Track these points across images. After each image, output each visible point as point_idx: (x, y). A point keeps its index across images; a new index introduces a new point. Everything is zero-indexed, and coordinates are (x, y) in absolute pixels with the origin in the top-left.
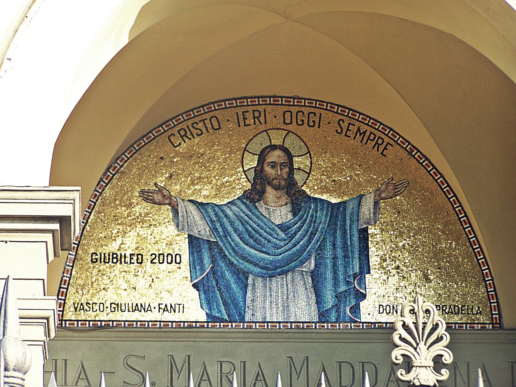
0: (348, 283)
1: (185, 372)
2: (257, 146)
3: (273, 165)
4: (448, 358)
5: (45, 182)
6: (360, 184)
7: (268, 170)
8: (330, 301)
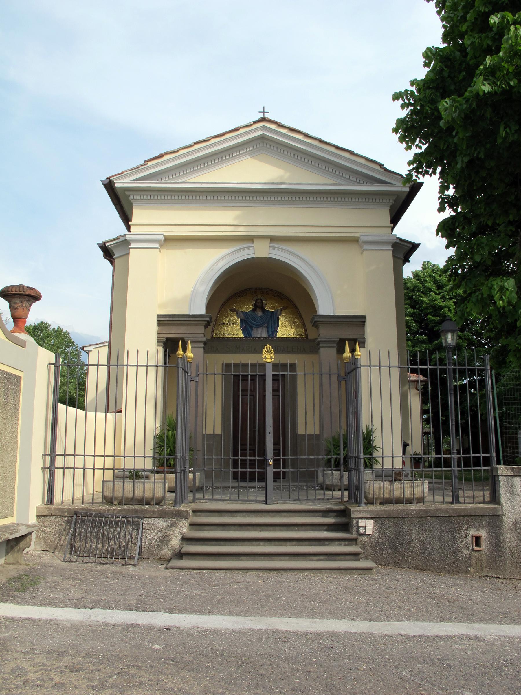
0: (275, 329)
2: (256, 298)
3: (258, 303)
4: (273, 357)
6: (277, 307)
8: (270, 333)
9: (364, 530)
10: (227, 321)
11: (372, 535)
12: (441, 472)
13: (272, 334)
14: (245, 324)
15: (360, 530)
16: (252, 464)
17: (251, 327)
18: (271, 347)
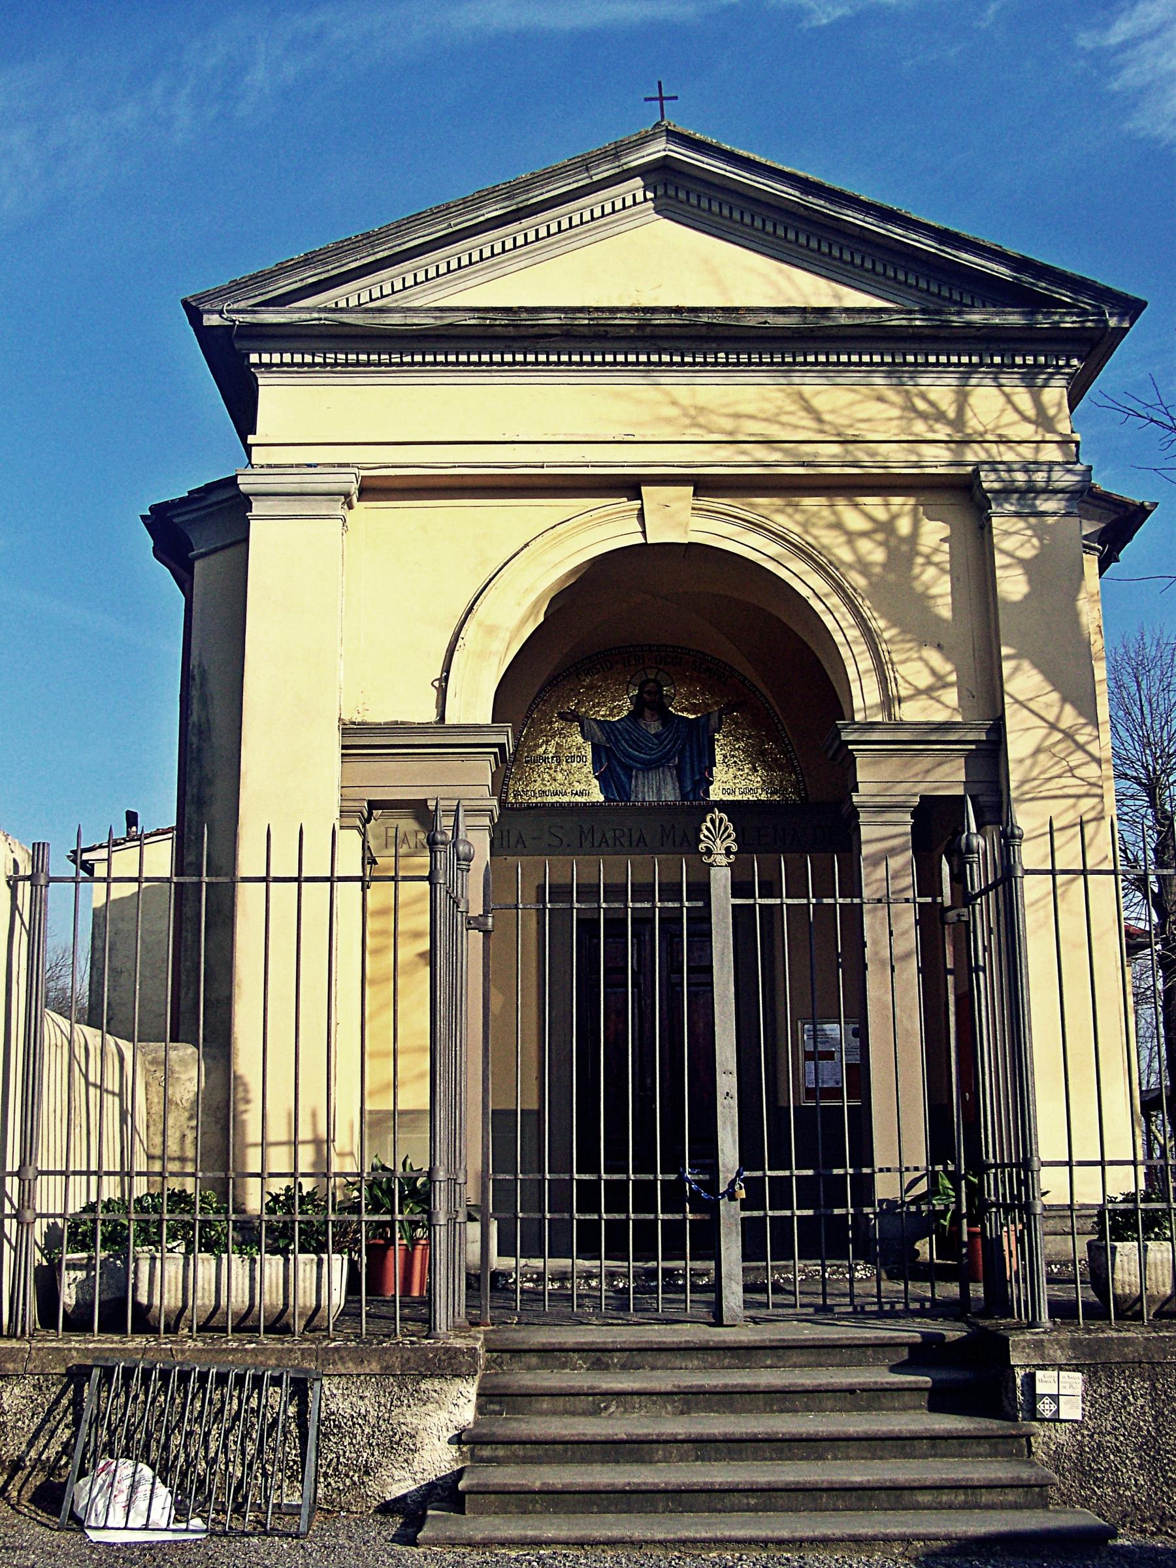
1: (590, 838)
3: (649, 693)
4: (735, 848)
5: (489, 722)
6: (708, 705)
7: (645, 696)
9: (1054, 1407)
10: (552, 749)
11: (1080, 1423)
12: (495, 1304)
13: (694, 790)
14: (609, 760)
15: (1040, 1406)
16: (674, 1197)
17: (628, 770)
18: (725, 816)
